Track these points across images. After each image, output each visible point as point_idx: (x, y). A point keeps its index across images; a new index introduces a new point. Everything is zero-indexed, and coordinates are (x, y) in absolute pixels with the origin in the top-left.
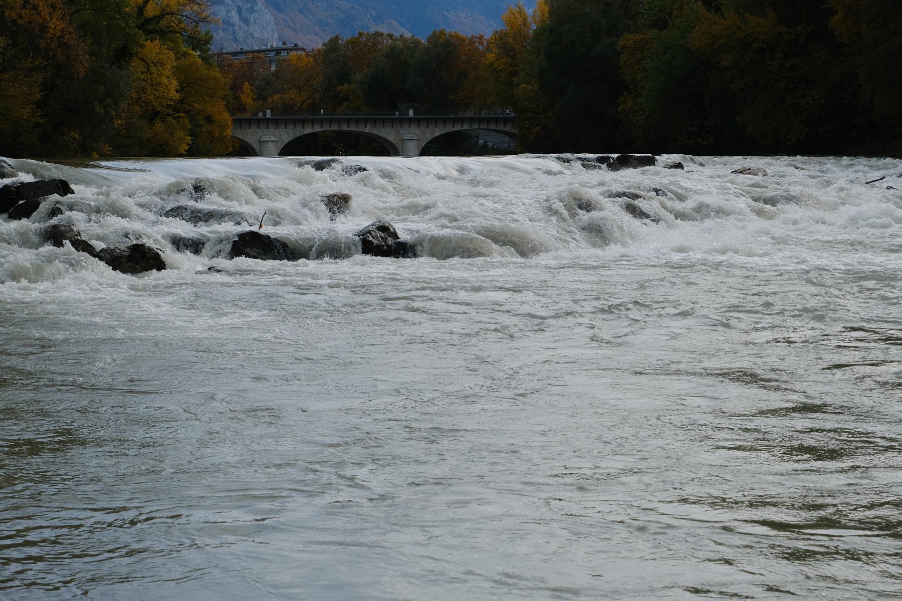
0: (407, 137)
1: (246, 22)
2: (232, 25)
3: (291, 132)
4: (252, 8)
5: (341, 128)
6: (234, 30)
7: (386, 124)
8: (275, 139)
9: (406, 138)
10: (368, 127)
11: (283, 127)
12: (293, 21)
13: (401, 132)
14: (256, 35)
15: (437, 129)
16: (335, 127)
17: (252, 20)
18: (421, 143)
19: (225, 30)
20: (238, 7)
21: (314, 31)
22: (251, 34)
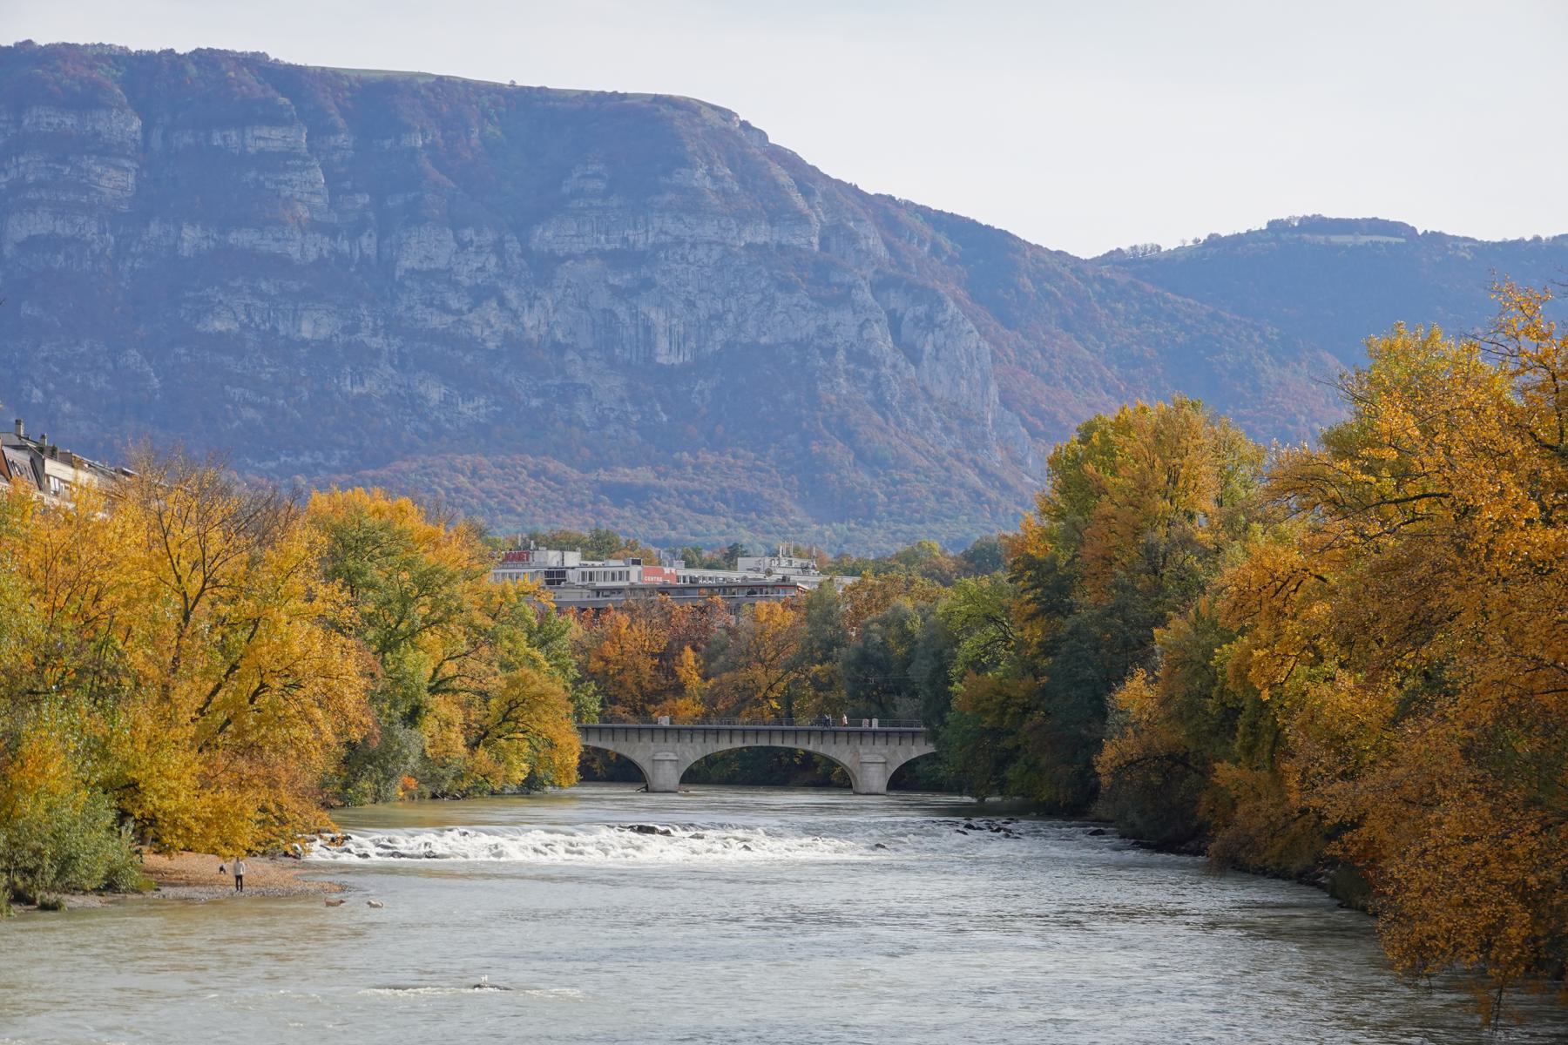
0: (867, 758)
1: (914, 357)
2: (874, 363)
3: (698, 748)
4: (930, 318)
5: (773, 744)
6: (877, 377)
7: (838, 739)
8: (675, 758)
9: (866, 760)
10: (811, 742)
11: (688, 740)
12: (1043, 352)
13: (861, 751)
14: (938, 392)
15: (914, 747)
16: (763, 742)
17: (928, 349)
18: (889, 767)
19: (855, 377)
20: (891, 314)
21: (1102, 380)
22: (924, 389)
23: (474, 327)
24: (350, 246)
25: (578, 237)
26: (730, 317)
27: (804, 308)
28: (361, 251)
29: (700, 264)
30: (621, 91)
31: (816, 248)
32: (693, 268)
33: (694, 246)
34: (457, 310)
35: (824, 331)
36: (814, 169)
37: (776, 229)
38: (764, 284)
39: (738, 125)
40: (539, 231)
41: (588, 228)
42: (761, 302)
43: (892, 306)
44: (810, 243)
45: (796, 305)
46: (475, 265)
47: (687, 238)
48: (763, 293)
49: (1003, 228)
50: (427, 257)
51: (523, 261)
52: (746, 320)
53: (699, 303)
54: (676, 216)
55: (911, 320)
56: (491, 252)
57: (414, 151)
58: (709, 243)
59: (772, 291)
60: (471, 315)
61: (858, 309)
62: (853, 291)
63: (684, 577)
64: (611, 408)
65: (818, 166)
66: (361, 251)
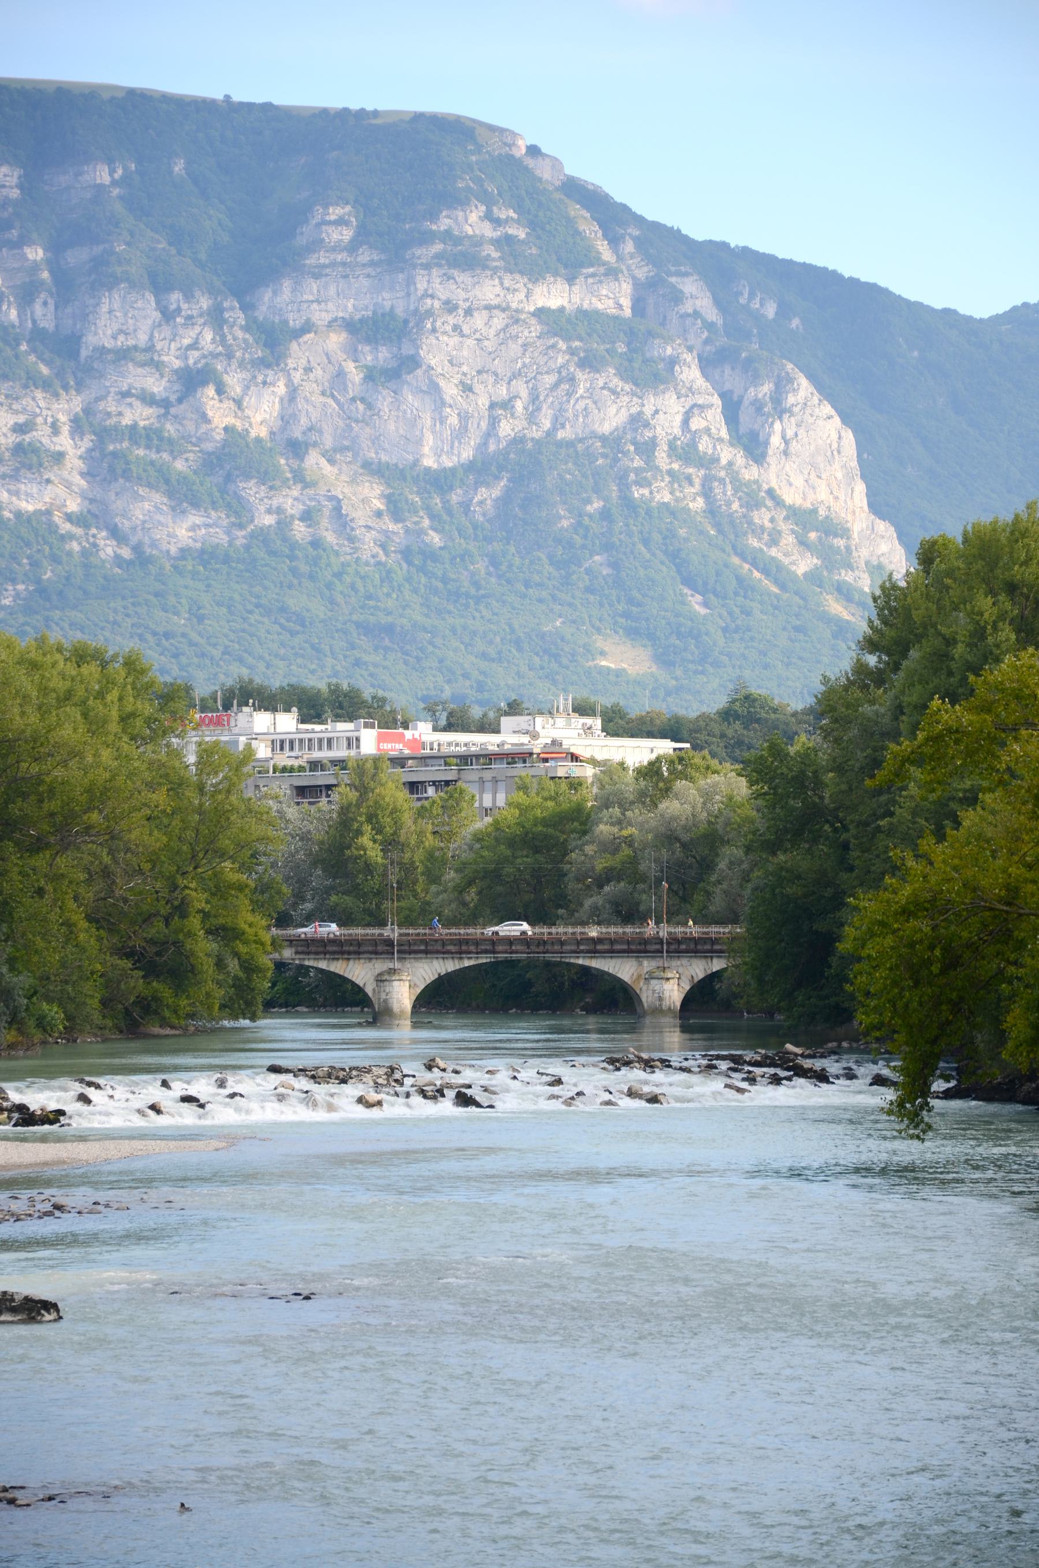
17: (776, 441)
23: (185, 422)
24: (19, 316)
25: (319, 302)
26: (519, 405)
27: (613, 392)
28: (34, 322)
29: (478, 336)
30: (369, 108)
31: (628, 312)
32: (471, 342)
33: (468, 312)
34: (163, 400)
35: (637, 421)
36: (625, 208)
37: (576, 289)
38: (560, 360)
39: (524, 151)
40: (268, 295)
41: (332, 290)
42: (556, 386)
43: (728, 386)
44: (620, 307)
45: (602, 388)
46: (187, 341)
47: (461, 303)
48: (559, 372)
49: (871, 280)
50: (121, 331)
51: (247, 336)
52: (539, 409)
53: (478, 388)
54: (445, 274)
55: (752, 404)
56: (204, 324)
57: (100, 188)
58: (488, 308)
59: (572, 369)
60: (182, 407)
61: (683, 392)
62: (677, 368)
63: (432, 744)
64: (367, 527)
65: (628, 204)
66: (34, 322)
